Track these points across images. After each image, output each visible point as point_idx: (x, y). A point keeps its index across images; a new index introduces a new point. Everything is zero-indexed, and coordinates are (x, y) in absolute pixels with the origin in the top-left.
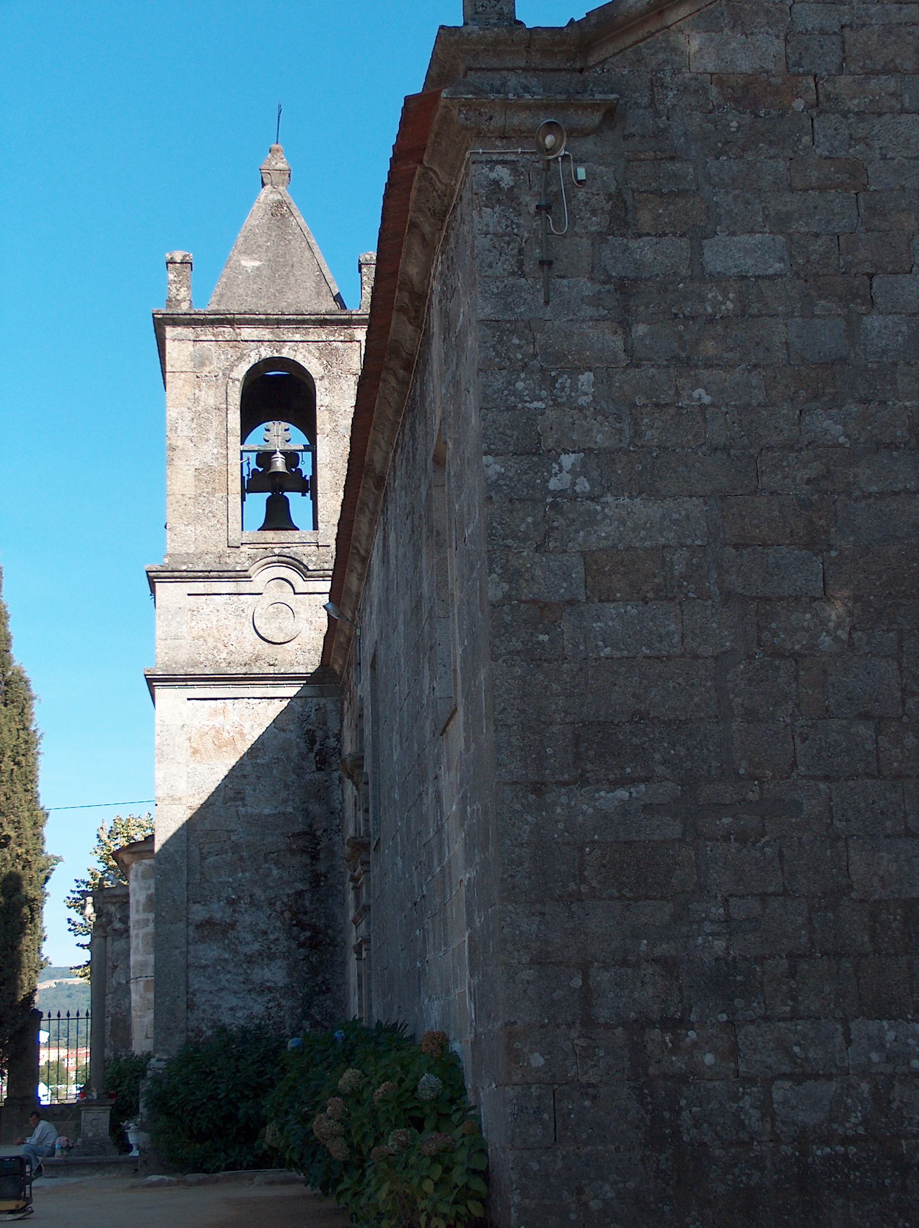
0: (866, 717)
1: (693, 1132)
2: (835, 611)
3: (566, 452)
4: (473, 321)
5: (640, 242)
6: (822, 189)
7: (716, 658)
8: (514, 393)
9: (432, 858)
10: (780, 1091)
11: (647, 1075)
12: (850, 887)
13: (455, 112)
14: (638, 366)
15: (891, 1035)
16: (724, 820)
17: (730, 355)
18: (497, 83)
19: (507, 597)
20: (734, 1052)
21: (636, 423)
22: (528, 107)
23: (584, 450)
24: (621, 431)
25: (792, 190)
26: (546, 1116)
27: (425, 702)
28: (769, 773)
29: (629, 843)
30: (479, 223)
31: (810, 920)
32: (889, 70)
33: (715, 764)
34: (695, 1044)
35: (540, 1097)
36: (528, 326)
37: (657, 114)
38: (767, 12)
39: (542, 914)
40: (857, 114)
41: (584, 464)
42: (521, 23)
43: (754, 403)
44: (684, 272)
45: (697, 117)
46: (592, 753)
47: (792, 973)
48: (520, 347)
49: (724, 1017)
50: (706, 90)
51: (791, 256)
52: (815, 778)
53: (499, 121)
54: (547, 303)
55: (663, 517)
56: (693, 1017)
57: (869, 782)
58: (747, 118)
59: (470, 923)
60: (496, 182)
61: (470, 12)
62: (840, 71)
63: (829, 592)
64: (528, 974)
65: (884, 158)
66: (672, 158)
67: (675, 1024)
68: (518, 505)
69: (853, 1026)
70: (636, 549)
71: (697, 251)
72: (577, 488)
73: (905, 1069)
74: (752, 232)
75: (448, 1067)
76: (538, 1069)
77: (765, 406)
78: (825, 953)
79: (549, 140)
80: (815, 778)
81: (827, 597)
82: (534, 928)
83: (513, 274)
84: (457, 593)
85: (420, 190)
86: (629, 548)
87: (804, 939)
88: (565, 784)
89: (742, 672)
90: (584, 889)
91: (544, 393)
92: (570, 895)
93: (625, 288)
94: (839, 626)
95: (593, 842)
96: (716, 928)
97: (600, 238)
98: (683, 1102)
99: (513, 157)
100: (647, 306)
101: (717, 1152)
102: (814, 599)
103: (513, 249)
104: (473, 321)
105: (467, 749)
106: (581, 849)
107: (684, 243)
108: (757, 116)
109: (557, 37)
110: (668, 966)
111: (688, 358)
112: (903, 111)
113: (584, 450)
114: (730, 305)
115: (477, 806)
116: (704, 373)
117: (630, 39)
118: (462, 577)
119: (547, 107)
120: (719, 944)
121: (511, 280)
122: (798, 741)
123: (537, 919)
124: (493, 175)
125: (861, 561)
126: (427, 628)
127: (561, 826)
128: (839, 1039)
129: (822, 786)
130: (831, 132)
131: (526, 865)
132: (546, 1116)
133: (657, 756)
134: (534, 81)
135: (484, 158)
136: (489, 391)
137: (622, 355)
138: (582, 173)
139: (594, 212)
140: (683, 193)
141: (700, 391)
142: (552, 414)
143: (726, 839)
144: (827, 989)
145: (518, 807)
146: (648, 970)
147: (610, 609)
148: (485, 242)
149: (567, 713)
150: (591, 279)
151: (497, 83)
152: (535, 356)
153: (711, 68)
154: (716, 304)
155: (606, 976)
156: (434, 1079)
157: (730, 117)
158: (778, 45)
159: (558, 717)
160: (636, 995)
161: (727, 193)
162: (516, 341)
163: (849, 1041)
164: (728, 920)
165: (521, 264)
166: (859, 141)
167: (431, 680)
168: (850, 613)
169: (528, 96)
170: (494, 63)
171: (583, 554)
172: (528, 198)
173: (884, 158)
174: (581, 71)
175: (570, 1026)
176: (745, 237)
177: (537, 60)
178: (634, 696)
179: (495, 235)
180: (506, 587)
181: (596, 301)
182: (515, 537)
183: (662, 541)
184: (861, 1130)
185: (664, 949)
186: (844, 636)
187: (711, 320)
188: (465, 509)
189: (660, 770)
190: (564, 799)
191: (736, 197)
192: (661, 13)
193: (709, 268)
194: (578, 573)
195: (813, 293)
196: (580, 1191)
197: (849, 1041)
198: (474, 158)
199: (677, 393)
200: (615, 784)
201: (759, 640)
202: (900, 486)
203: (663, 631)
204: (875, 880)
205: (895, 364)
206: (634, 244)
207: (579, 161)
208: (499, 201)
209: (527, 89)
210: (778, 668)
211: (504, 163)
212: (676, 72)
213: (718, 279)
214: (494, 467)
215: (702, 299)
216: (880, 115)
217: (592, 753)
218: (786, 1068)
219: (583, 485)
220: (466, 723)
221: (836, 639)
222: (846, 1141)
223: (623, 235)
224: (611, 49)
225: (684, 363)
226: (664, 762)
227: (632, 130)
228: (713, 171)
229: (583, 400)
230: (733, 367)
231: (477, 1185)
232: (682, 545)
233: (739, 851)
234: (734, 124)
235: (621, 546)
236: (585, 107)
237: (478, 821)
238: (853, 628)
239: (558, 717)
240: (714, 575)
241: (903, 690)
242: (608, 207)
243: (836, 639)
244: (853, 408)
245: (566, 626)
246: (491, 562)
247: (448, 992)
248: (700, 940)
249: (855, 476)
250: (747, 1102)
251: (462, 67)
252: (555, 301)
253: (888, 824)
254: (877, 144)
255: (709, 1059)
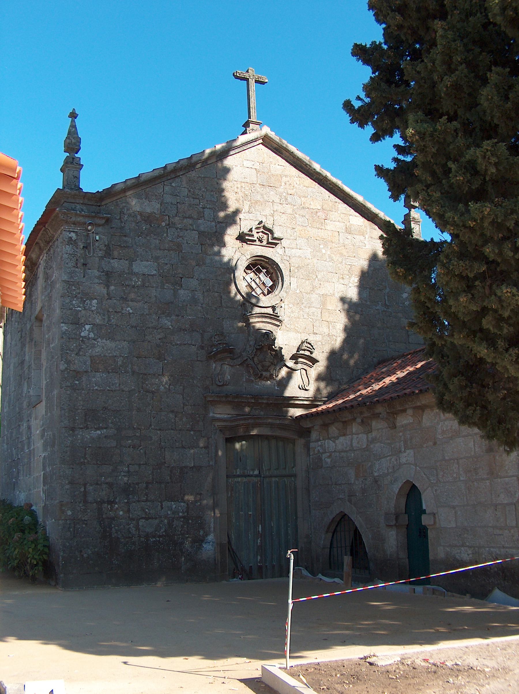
0: (172, 412)
1: (115, 534)
2: (165, 379)
3: (87, 324)
4: (60, 280)
5: (114, 261)
6: (169, 250)
7: (129, 392)
8: (72, 304)
9: (24, 447)
10: (142, 522)
11: (102, 517)
12: (165, 462)
13: (60, 215)
14: (111, 299)
15: (174, 506)
16: (129, 441)
17: (139, 298)
18: (73, 207)
19: (66, 369)
20: (129, 511)
21: (109, 317)
22: (83, 216)
23: (92, 324)
24: (104, 319)
25: (160, 249)
26: (71, 529)
27: (24, 395)
28: (143, 428)
29: (100, 448)
30: (63, 250)
31: (153, 472)
32: (190, 217)
33: (127, 424)
34: (117, 508)
35: (70, 524)
36: (78, 284)
37: (121, 222)
38: (156, 195)
39: (73, 468)
40: (180, 229)
41: (92, 328)
42: (81, 189)
43: (145, 313)
44: (126, 271)
45: (134, 224)
46: (90, 419)
47: (147, 488)
48: (75, 290)
49: (126, 501)
50: (136, 217)
51: (158, 269)
52: (156, 429)
53: (73, 219)
54: (84, 277)
55: (116, 347)
56: (117, 501)
57: (172, 431)
58: (148, 226)
59: (44, 469)
60: (71, 238)
61: (66, 183)
62: (176, 216)
63: (164, 373)
64: (67, 487)
65: (187, 243)
66: (125, 236)
67: (111, 503)
68: (71, 340)
69: (163, 504)
70: (107, 356)
71: (131, 265)
72: (90, 336)
73: (177, 516)
74: (148, 261)
75: (33, 514)
76: (70, 515)
77: (148, 315)
78: (156, 482)
79: (90, 228)
80: (156, 429)
81: (163, 375)
82: (70, 473)
83: (74, 267)
84: (45, 364)
85: (42, 234)
86: (105, 356)
87: (151, 478)
88: (81, 428)
89: (137, 396)
90: (86, 461)
91: (81, 305)
92: (81, 463)
93: (108, 274)
94: (166, 383)
95: (89, 447)
96: (125, 474)
97: (101, 258)
98: (113, 526)
99: (76, 230)
100: (115, 280)
101: (122, 540)
102: (159, 375)
103: (74, 259)
104: (60, 280)
105: (46, 414)
106: (85, 449)
107: (127, 262)
108: (151, 226)
109: (94, 196)
110: (110, 485)
111: (126, 298)
112: (193, 230)
113: (92, 324)
114: (140, 283)
115: (50, 433)
116: (130, 303)
117: (115, 198)
118: (48, 359)
119: (89, 217)
120: (126, 479)
121: (73, 269)
122: (152, 418)
123: (71, 470)
124: (70, 235)
125: (174, 364)
126: (27, 371)
127: (79, 441)
128: (159, 507)
129: (158, 432)
130: (172, 233)
131: (68, 453)
132: (71, 529)
133: (110, 421)
134: (85, 208)
135: (68, 230)
136: (64, 303)
137: (106, 295)
138: (97, 238)
139: (100, 250)
140: (128, 247)
141: (129, 309)
142: (83, 312)
143: (129, 447)
144: (157, 493)
145: (67, 435)
146: (104, 486)
147: (98, 374)
148: (66, 256)
149: (83, 406)
150: (98, 271)
151: (73, 207)
152: (79, 293)
153: (138, 210)
154: (136, 282)
155: (91, 488)
156: (29, 518)
157: (143, 225)
158: (159, 206)
159: (80, 407)
160: (100, 494)
161: (141, 248)
162: (74, 288)
163: (162, 508)
164: (129, 472)
165: (77, 264)
166: (181, 237)
167: (28, 388)
168: (170, 380)
169: (83, 213)
170: (73, 201)
171: (91, 357)
172: (80, 244)
173: (187, 243)
174: (99, 206)
175: (80, 502)
176: (145, 262)
177: (86, 201)
178: (104, 402)
179: (70, 254)
180: (66, 365)
181: (99, 278)
182: (70, 350)
183: (115, 354)
184: (164, 534)
185: (109, 480)
186: (168, 387)
187: (134, 287)
188: (51, 338)
189: (110, 425)
190: (81, 433)
191: (143, 250)
192: (125, 192)
193: (134, 271)
194: (89, 363)
195: (164, 282)
196: (81, 551)
197: (162, 508)
198: (65, 229)
199: (122, 309)
200: (99, 429)
201: (142, 387)
202: (186, 342)
203: (113, 382)
204: (172, 460)
205: (187, 305)
206: (112, 261)
207: (97, 234)
208: (71, 244)
209: (82, 210)
210: (147, 396)
211: (73, 232)
212: (128, 210)
213: (136, 274)
214: (64, 327)
215: (131, 280)
216: (187, 230)
217: (90, 419)
218: (144, 516)
219: (92, 335)
220: (46, 406)
221: (165, 388)
222: (160, 536)
223: (109, 258)
224: (109, 201)
225: (124, 299)
226: (112, 423)
227: (114, 226)
228: (137, 241)
229: (93, 308)
230: (140, 302)
231: (46, 550)
232: (121, 356)
233: (133, 451)
234: (144, 227)
235: (102, 355)
236: (100, 218)
237: (50, 438)
238: (170, 385)
239: (80, 407)
240: (130, 366)
241: (184, 404)
242: (105, 249)
243: (165, 388)
244: (174, 317)
245: (84, 379)
246: (62, 357)
247: (30, 490)
248: (120, 477)
249: (174, 338)
250: (132, 525)
251: (63, 201)
252: (86, 276)
253: (177, 444)
254: (185, 239)
255: (121, 513)
